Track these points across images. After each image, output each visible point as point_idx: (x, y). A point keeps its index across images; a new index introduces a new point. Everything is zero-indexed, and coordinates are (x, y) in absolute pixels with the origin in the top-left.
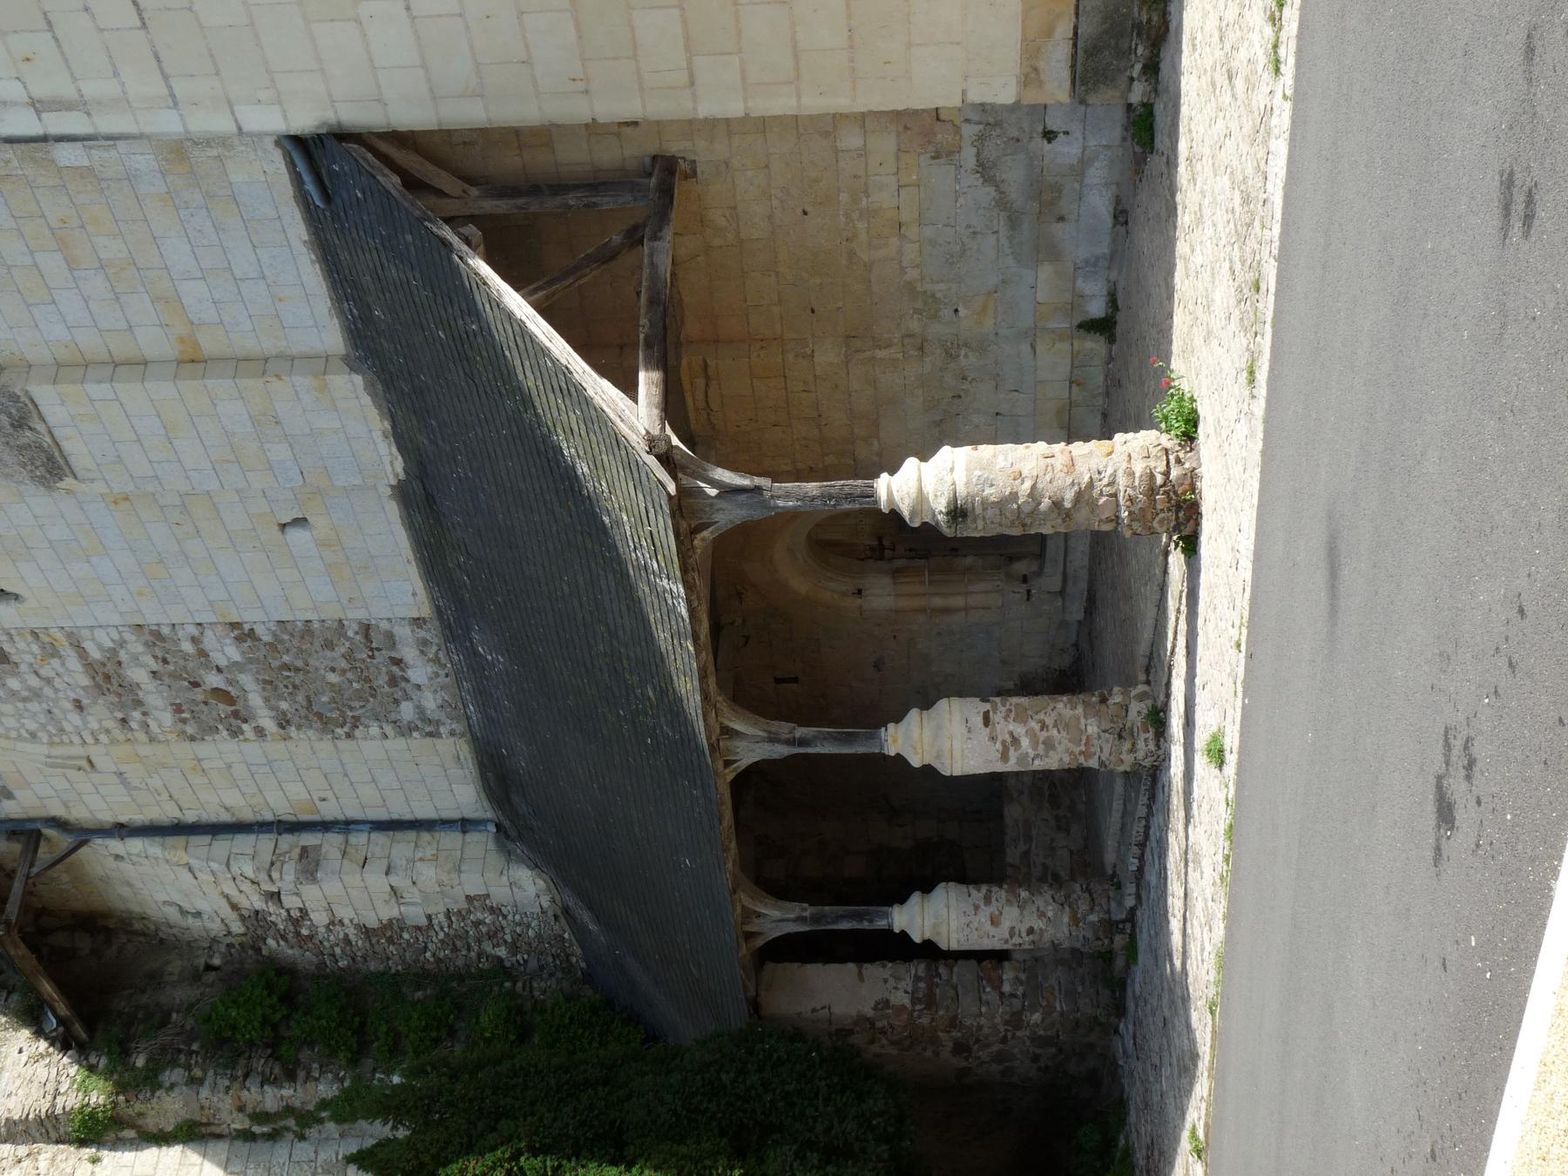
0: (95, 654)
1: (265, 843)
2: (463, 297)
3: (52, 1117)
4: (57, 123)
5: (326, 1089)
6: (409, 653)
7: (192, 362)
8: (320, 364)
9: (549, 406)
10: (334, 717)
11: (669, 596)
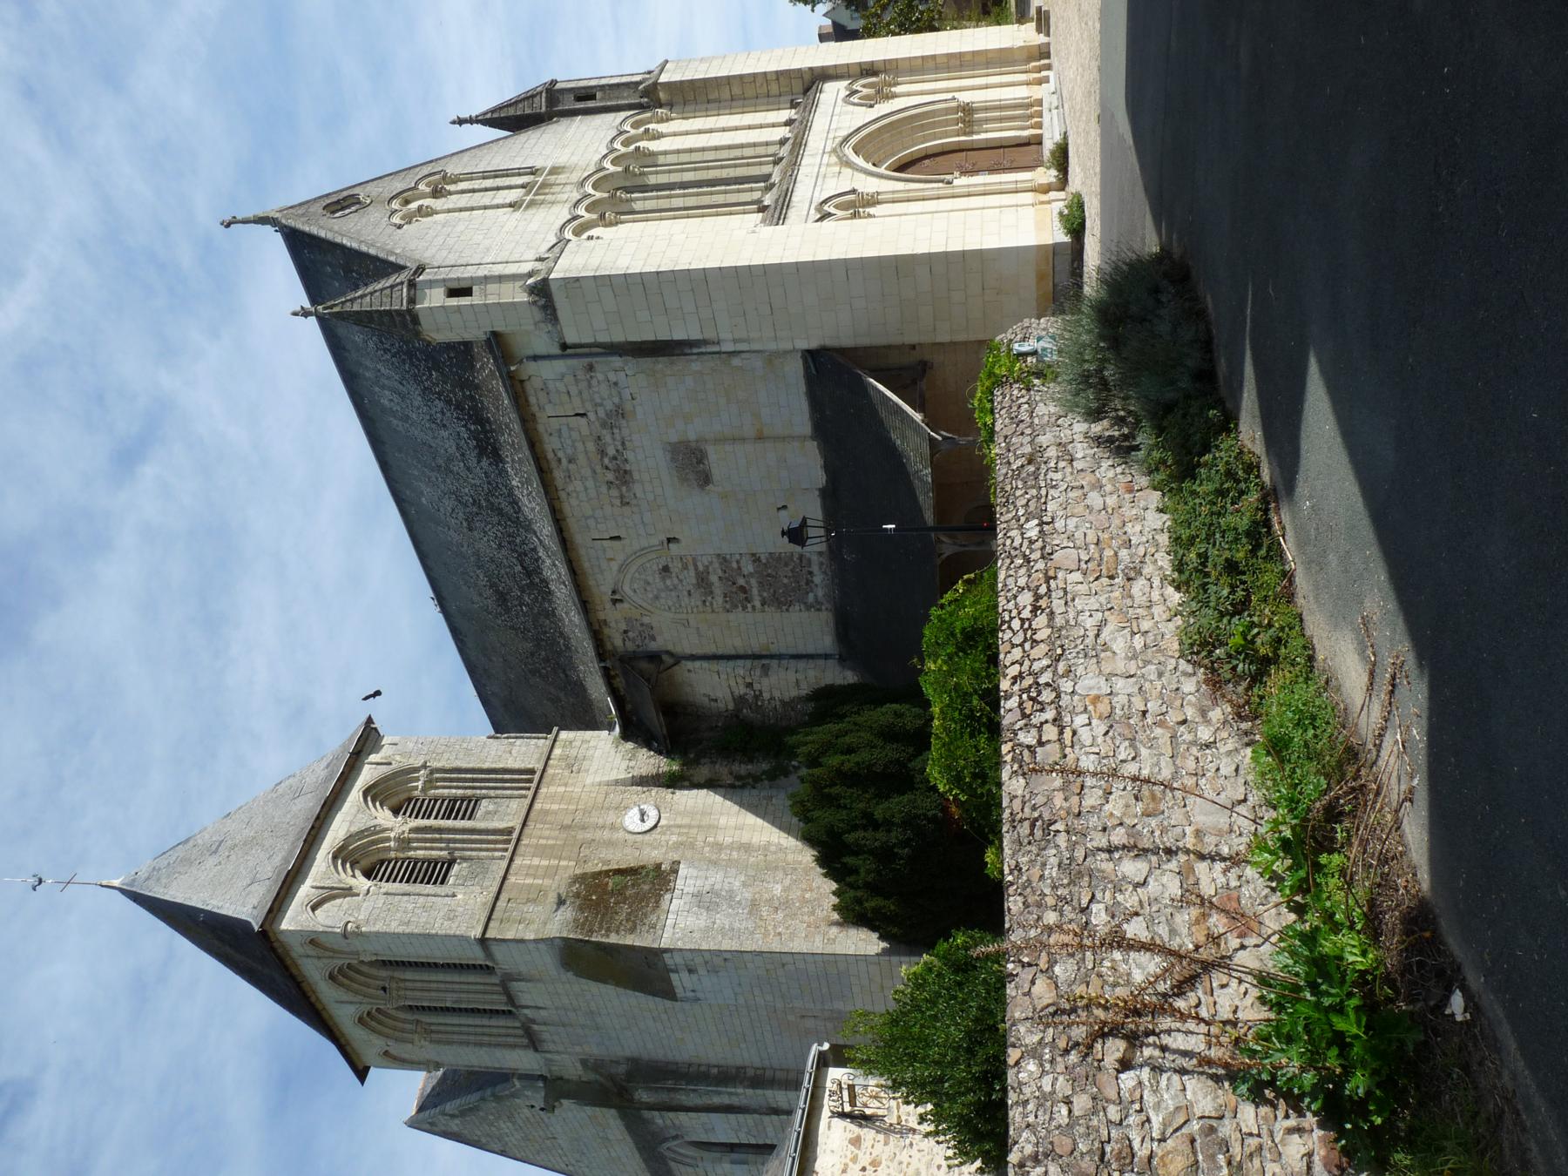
0: (701, 568)
1: (748, 663)
2: (865, 389)
3: (658, 775)
5: (765, 766)
6: (815, 568)
7: (760, 438)
8: (803, 438)
9: (891, 421)
10: (779, 600)
11: (924, 473)
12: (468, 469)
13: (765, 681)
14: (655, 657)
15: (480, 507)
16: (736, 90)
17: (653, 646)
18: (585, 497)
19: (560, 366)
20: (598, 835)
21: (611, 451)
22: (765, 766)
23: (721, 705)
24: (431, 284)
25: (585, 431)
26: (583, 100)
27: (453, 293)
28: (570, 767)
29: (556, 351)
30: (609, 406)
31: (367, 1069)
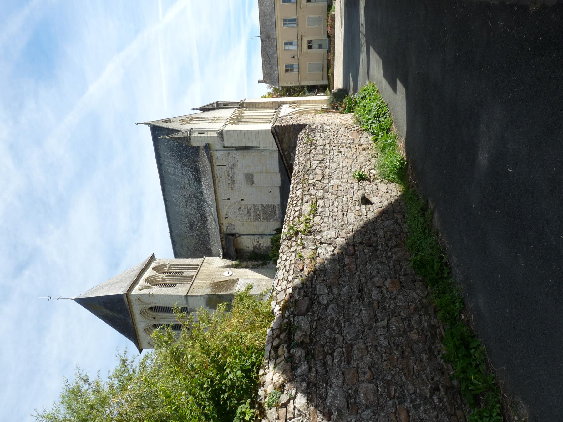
4: (265, 149)
5: (261, 262)
6: (277, 209)
7: (267, 172)
8: (276, 173)
12: (190, 187)
13: (262, 240)
14: (233, 235)
15: (191, 197)
16: (263, 105)
17: (234, 231)
18: (222, 186)
19: (222, 153)
20: (217, 276)
21: (231, 175)
22: (261, 262)
23: (250, 249)
24: (195, 131)
25: (225, 170)
26: (225, 105)
27: (199, 134)
28: (209, 264)
29: (222, 148)
30: (232, 163)
31: (142, 349)
